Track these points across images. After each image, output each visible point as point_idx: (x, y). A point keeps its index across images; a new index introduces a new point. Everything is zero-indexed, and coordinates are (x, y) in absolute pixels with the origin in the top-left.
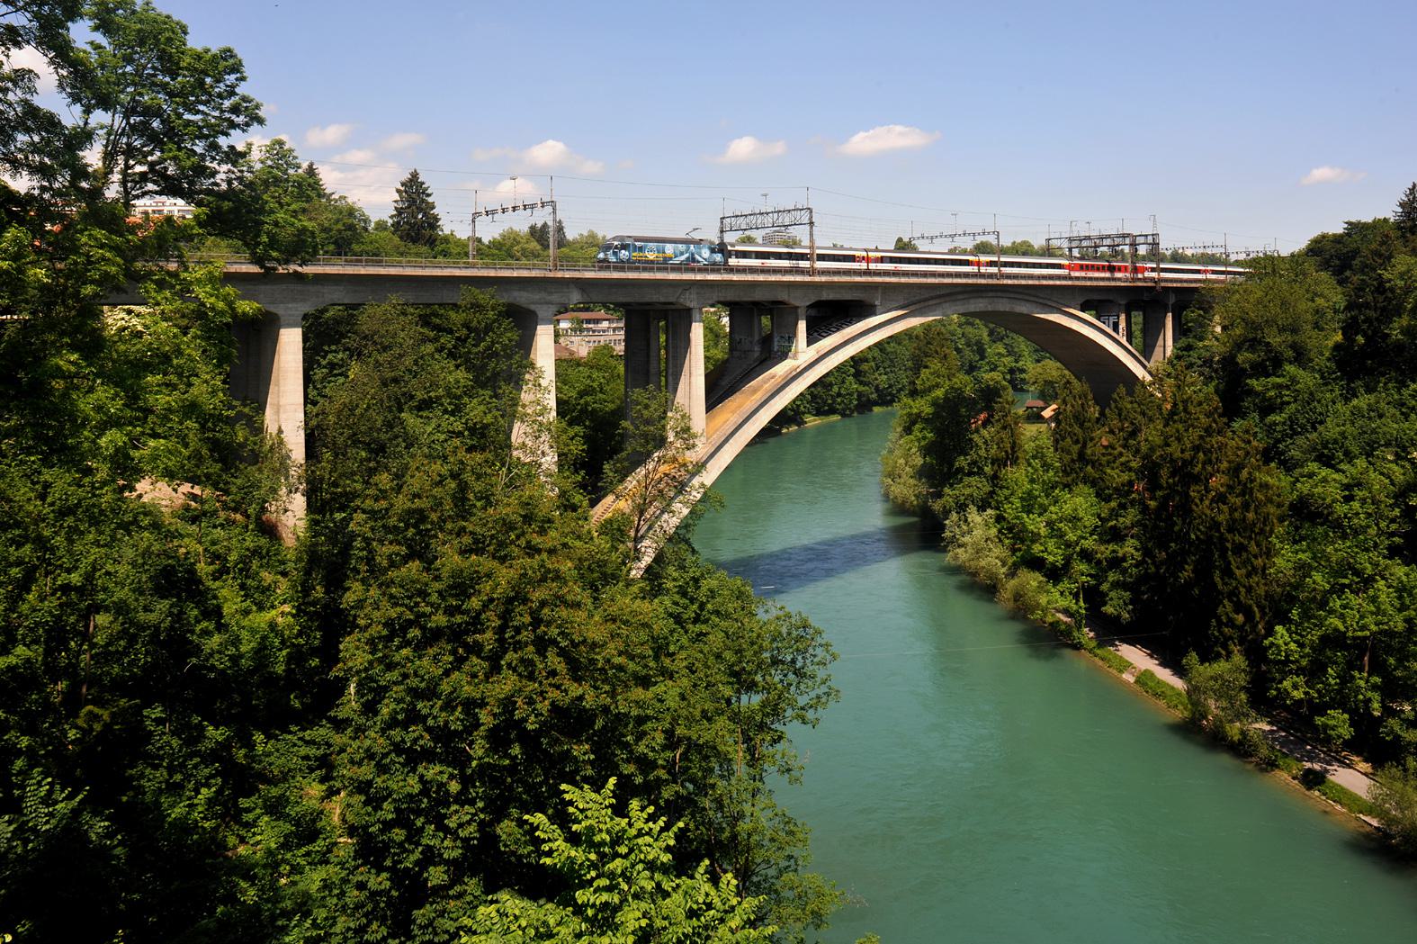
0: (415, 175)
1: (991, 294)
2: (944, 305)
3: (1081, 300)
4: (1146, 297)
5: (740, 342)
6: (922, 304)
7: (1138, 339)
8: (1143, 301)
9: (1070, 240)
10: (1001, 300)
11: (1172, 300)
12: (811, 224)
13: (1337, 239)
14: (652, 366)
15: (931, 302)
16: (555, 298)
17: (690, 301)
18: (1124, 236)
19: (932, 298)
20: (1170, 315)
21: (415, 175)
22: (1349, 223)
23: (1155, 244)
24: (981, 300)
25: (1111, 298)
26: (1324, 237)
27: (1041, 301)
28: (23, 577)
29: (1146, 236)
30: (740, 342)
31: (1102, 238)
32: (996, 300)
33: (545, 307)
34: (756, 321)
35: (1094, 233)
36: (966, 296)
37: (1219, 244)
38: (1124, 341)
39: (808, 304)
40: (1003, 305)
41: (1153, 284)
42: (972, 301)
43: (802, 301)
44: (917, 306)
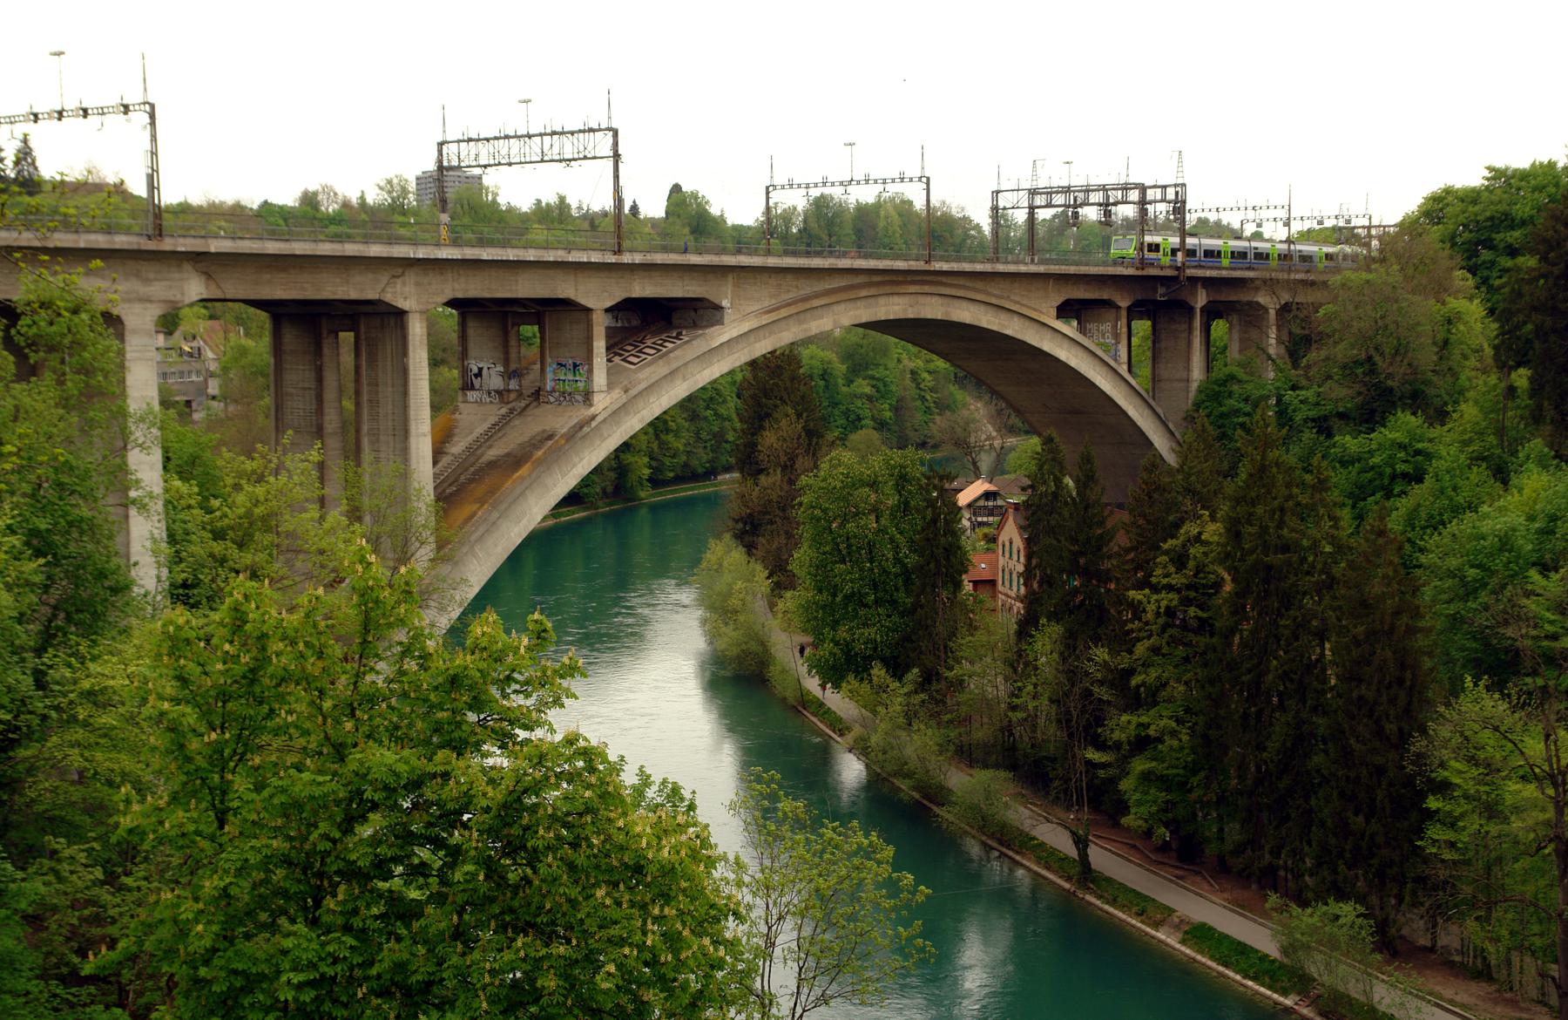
0: (676, 189)
1: (913, 289)
2: (835, 308)
3: (1058, 300)
4: (1161, 294)
5: (479, 374)
6: (801, 307)
7: (1145, 371)
8: (1155, 302)
9: (1033, 192)
10: (928, 299)
11: (1201, 299)
12: (616, 156)
13: (1471, 197)
14: (327, 418)
15: (816, 303)
16: (158, 289)
17: (405, 295)
18: (1126, 188)
19: (817, 296)
20: (1171, 459)
21: (676, 189)
22: (1491, 169)
23: (1179, 207)
24: (896, 299)
25: (1105, 297)
26: (1448, 191)
27: (994, 301)
28: (1397, 233)
29: (1165, 187)
30: (479, 374)
31: (1087, 190)
32: (921, 299)
33: (137, 308)
34: (513, 332)
35: (1078, 181)
36: (873, 291)
37: (1279, 204)
38: (1123, 369)
39: (609, 304)
40: (932, 308)
41: (1174, 273)
42: (882, 301)
43: (598, 297)
44: (792, 310)
